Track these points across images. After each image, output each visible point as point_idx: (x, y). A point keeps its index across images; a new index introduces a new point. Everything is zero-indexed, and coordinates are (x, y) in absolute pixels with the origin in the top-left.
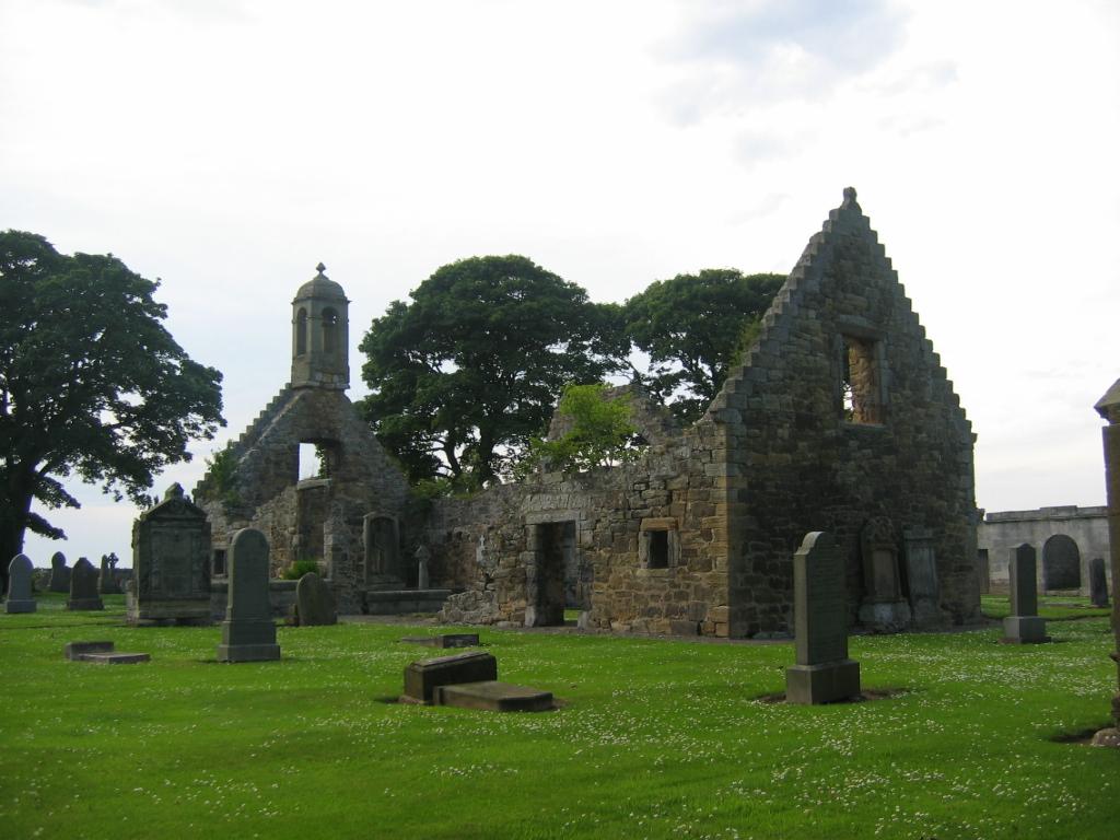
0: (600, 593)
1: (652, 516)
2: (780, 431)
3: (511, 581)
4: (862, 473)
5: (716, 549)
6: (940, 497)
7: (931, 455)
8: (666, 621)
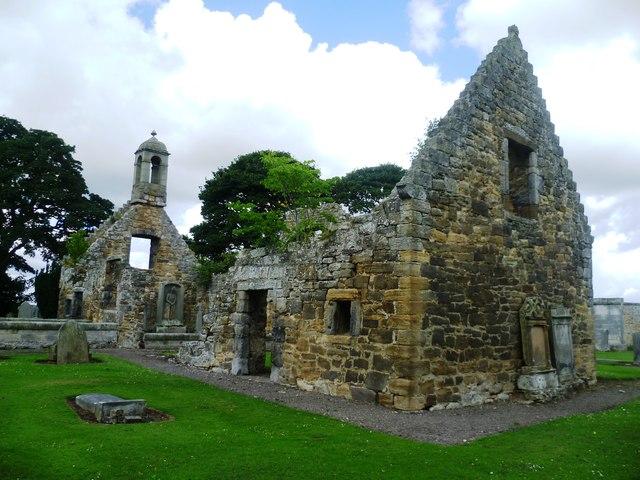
0: (290, 352)
1: (337, 287)
2: (459, 213)
3: (223, 336)
4: (520, 258)
6: (572, 284)
7: (567, 250)
8: (346, 386)
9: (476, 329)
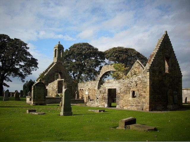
3: (102, 99)
5: (147, 95)
8: (135, 107)
9: (160, 96)
